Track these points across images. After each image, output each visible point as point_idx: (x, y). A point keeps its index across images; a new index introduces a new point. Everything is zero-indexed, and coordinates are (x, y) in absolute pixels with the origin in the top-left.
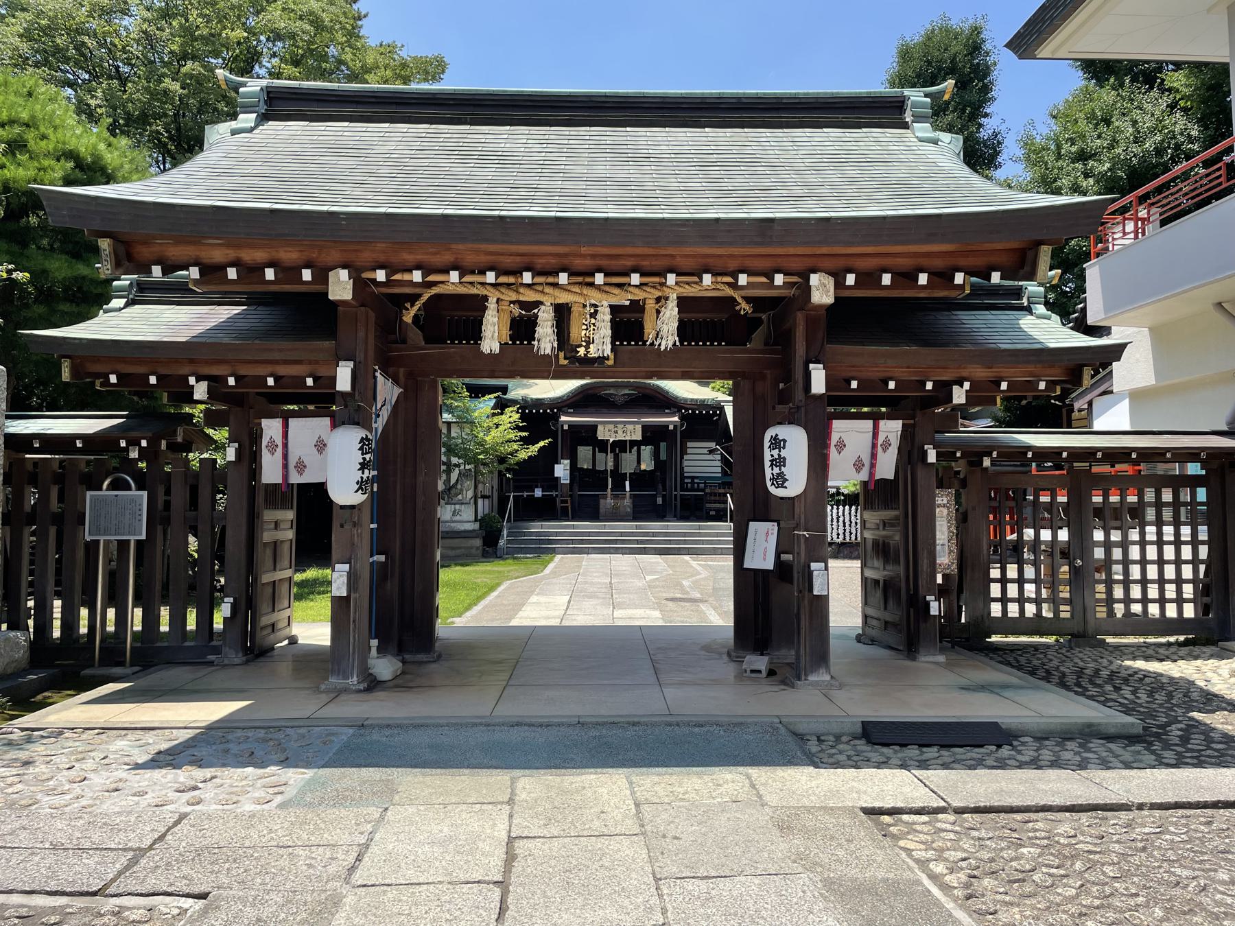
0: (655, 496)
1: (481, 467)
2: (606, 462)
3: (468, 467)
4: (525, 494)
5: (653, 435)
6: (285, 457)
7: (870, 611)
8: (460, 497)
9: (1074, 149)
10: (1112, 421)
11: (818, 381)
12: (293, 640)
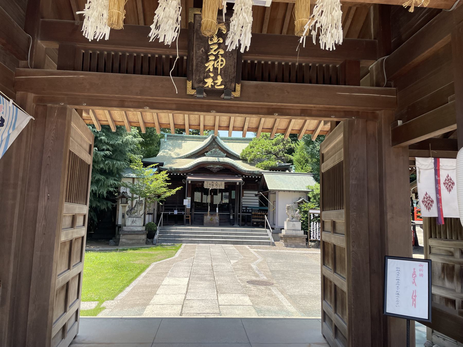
0: (229, 215)
1: (148, 200)
2: (207, 199)
3: (141, 199)
4: (170, 213)
5: (230, 187)
8: (136, 214)
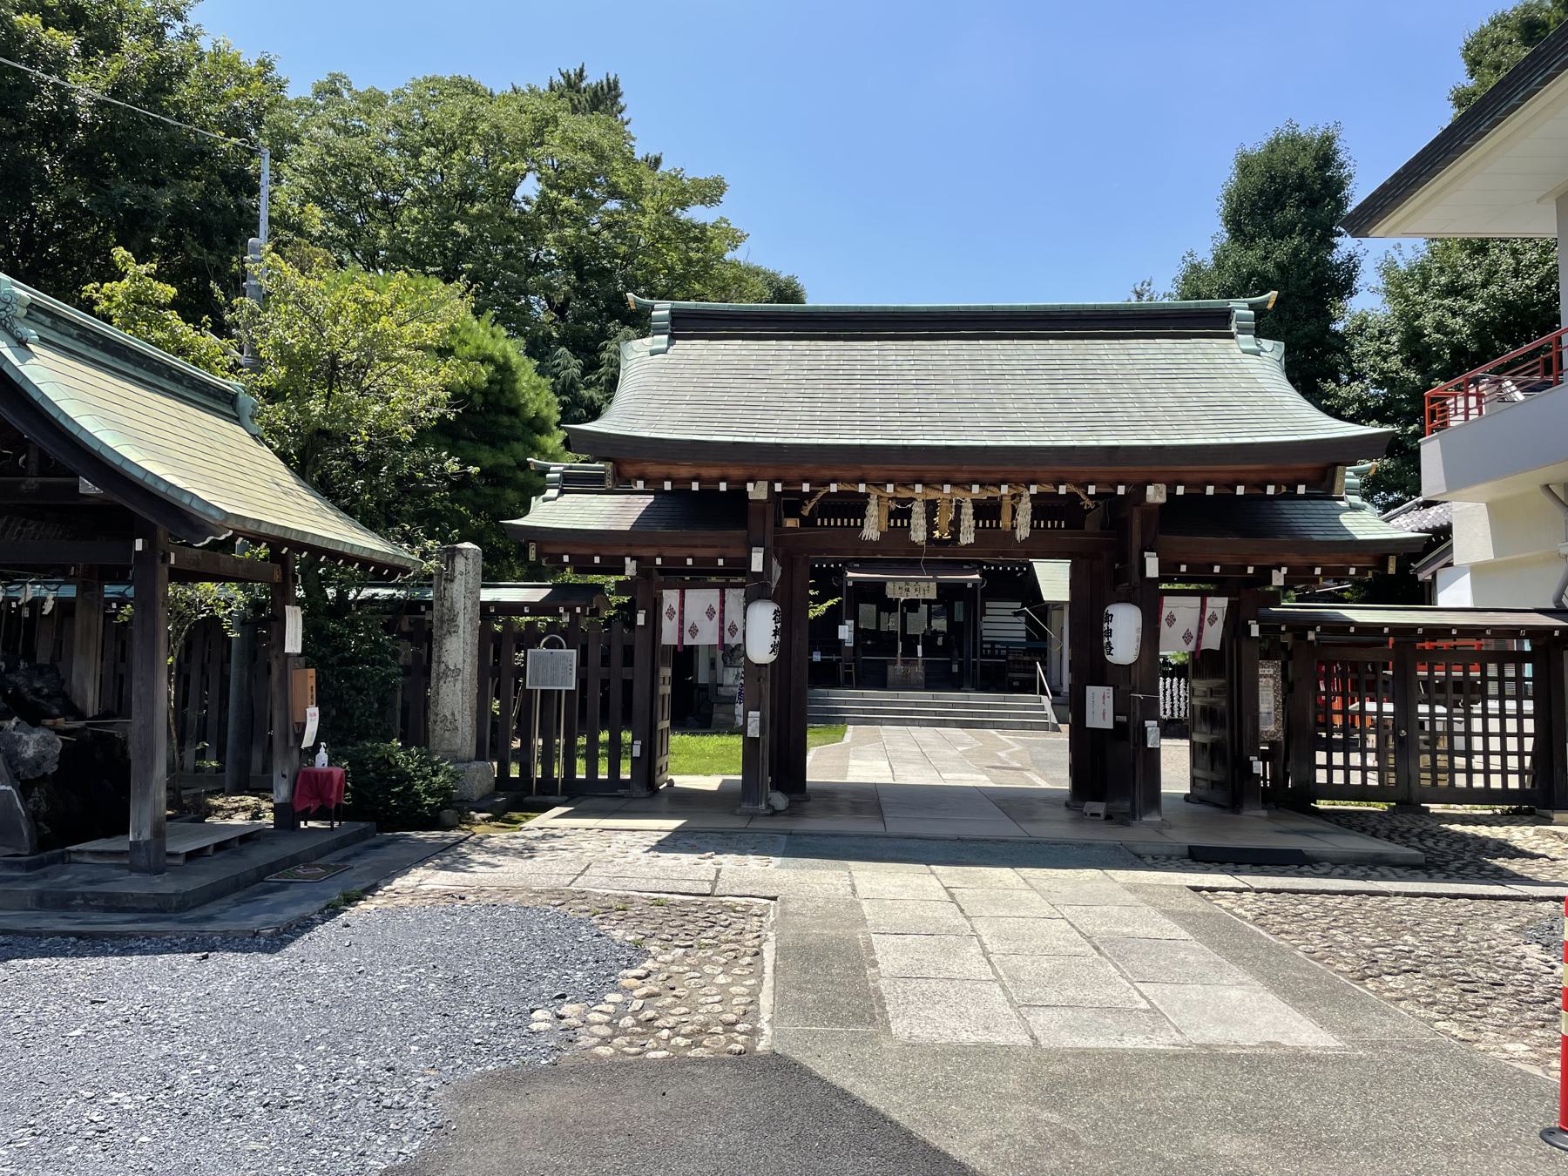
0: (950, 664)
2: (892, 623)
6: (681, 622)
7: (1199, 773)
9: (1443, 280)
10: (1455, 596)
11: (1152, 568)
12: (671, 783)
